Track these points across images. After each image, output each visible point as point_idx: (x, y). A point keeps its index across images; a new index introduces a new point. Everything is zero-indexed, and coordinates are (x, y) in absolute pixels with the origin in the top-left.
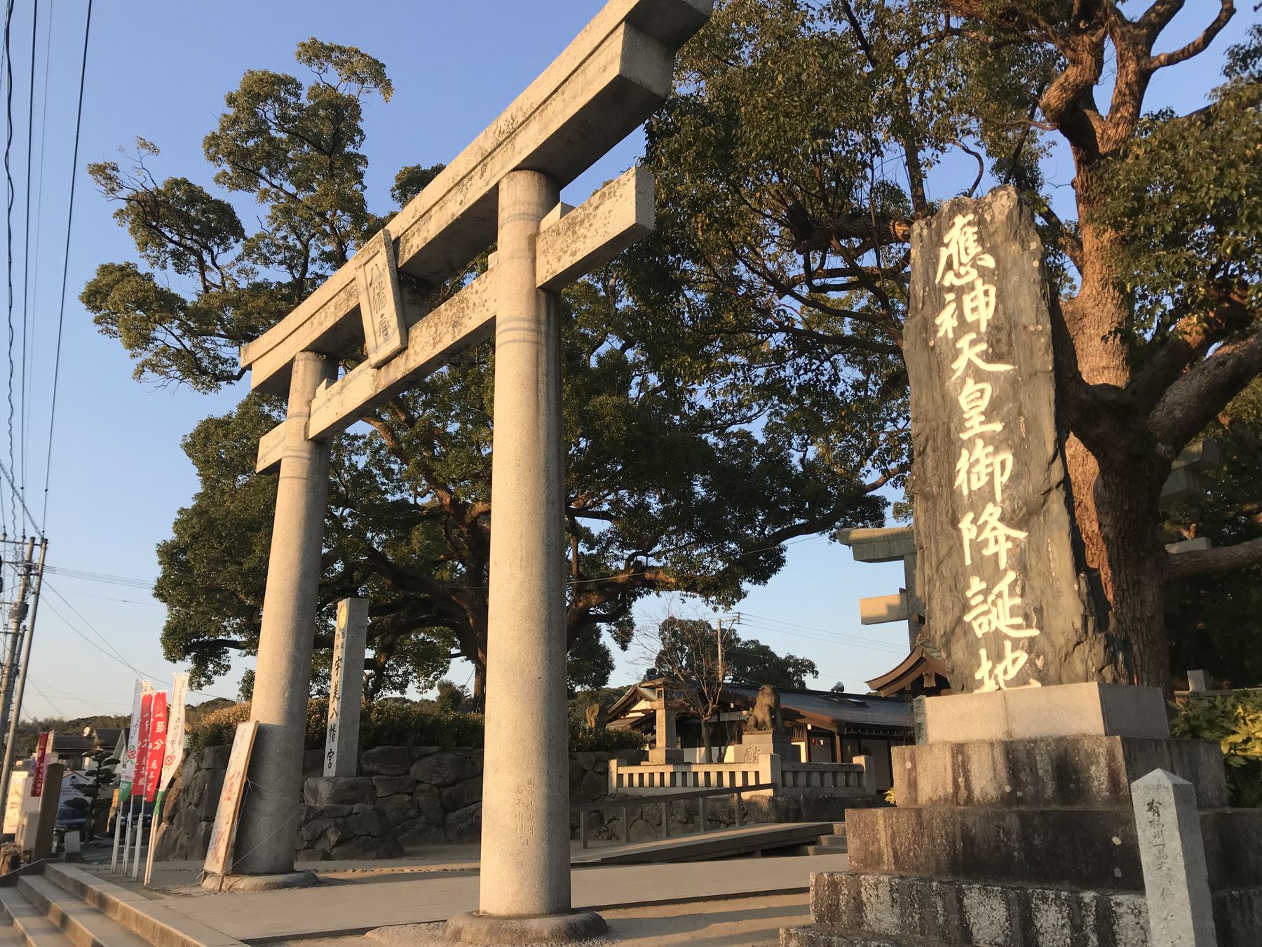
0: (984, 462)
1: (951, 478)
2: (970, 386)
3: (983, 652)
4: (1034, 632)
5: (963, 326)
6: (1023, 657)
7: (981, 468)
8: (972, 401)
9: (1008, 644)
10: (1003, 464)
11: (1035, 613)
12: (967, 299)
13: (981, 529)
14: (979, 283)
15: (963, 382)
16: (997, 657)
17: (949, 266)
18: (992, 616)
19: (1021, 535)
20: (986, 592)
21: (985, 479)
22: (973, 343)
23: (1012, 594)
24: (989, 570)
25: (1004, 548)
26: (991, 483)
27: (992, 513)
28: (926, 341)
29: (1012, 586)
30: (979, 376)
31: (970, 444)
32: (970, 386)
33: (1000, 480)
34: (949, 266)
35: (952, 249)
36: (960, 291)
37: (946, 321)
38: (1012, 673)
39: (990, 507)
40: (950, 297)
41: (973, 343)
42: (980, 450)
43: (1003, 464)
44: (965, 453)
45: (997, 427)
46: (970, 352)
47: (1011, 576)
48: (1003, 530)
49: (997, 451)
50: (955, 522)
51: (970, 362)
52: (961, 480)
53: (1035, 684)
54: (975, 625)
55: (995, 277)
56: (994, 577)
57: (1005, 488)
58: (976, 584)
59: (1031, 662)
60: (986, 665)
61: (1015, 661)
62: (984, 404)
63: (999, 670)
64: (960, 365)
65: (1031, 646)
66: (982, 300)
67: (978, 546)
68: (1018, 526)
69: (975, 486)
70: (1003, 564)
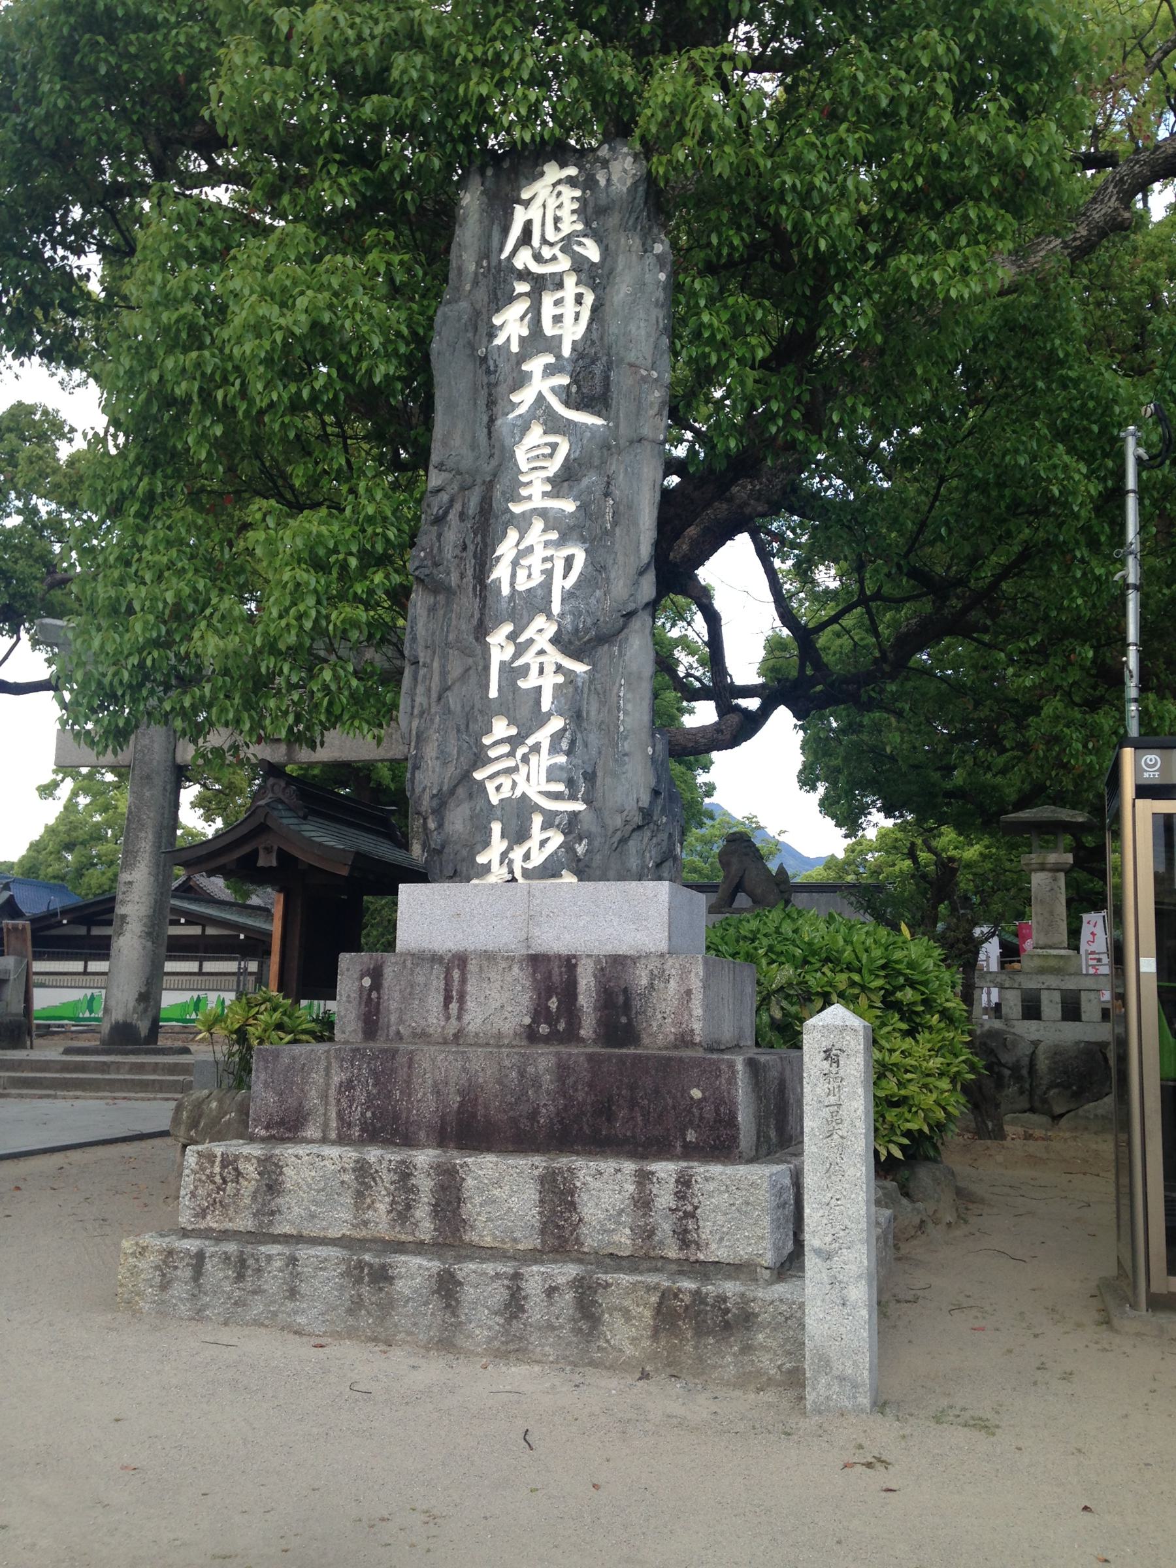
0: (540, 552)
1: (484, 561)
2: (536, 435)
3: (496, 828)
4: (579, 806)
5: (536, 341)
6: (557, 839)
7: (535, 561)
8: (537, 459)
9: (537, 820)
10: (569, 561)
11: (582, 778)
12: (548, 300)
13: (520, 650)
14: (570, 281)
15: (525, 429)
16: (518, 835)
17: (526, 237)
18: (520, 778)
19: (580, 668)
20: (515, 742)
21: (538, 578)
22: (549, 371)
23: (554, 749)
24: (524, 711)
25: (549, 682)
26: (547, 585)
27: (541, 630)
28: (472, 347)
29: (556, 738)
30: (554, 424)
31: (523, 523)
32: (536, 435)
33: (560, 584)
34: (526, 237)
35: (534, 212)
36: (540, 284)
37: (511, 324)
38: (537, 859)
39: (540, 621)
40: (522, 287)
41: (549, 371)
42: (536, 533)
43: (569, 561)
44: (513, 535)
45: (568, 506)
46: (541, 383)
47: (557, 724)
48: (554, 656)
49: (561, 542)
50: (482, 631)
51: (540, 398)
52: (501, 573)
53: (568, 878)
54: (490, 787)
55: (594, 276)
56: (527, 716)
57: (568, 596)
58: (501, 728)
59: (567, 846)
60: (498, 844)
61: (544, 843)
62: (554, 466)
63: (517, 854)
64: (524, 398)
65: (571, 826)
66: (569, 309)
67: (512, 673)
68: (577, 656)
69: (522, 585)
70: (546, 704)
